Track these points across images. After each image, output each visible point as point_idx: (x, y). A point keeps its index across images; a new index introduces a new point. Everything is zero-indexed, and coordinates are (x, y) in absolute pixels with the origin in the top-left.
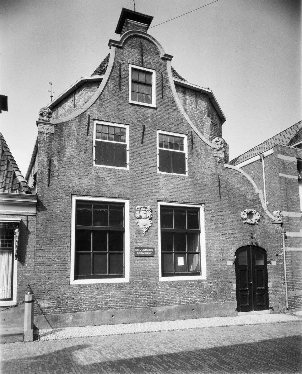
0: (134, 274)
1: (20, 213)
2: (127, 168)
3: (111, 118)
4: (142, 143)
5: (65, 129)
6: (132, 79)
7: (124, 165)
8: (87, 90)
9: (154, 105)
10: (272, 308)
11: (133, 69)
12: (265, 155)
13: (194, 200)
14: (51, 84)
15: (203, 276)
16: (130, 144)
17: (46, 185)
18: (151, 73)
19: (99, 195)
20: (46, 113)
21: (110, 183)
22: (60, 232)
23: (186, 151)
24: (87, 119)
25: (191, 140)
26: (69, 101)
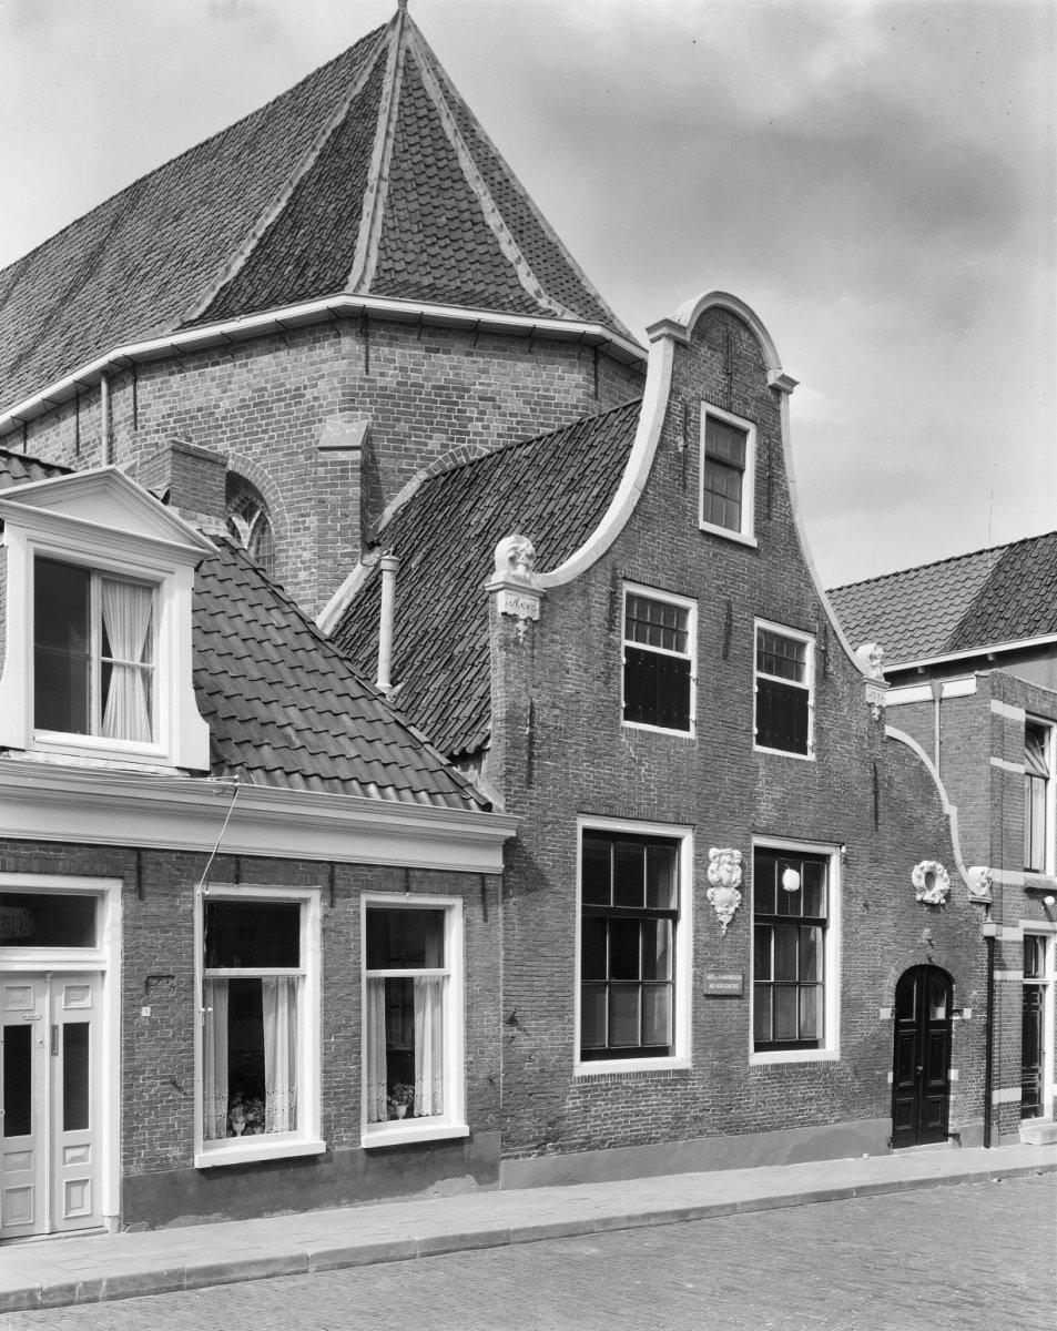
2: (691, 734)
4: (725, 657)
5: (562, 607)
6: (706, 452)
10: (956, 1136)
11: (710, 417)
15: (682, 1055)
16: (700, 660)
19: (635, 814)
20: (523, 554)
22: (552, 923)
23: (808, 681)
25: (822, 655)
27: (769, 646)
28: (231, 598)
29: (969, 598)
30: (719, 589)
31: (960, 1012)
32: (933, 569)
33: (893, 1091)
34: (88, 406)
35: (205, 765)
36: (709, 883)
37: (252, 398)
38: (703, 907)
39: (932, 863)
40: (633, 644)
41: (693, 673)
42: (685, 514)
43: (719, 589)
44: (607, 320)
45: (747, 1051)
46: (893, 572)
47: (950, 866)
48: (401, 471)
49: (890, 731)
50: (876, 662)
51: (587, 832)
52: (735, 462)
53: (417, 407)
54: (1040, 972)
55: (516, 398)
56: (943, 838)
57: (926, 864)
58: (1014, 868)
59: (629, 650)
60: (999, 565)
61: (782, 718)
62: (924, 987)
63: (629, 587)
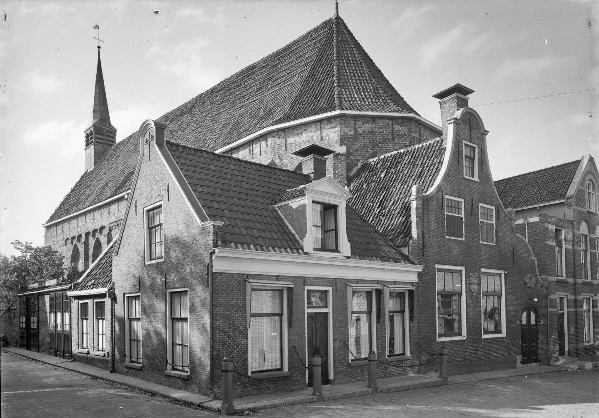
10: (540, 361)
16: (465, 217)
28: (267, 187)
30: (469, 195)
31: (540, 322)
35: (349, 255)
37: (309, 140)
40: (482, 220)
43: (469, 195)
44: (411, 110)
45: (305, 309)
48: (356, 160)
53: (361, 140)
56: (533, 268)
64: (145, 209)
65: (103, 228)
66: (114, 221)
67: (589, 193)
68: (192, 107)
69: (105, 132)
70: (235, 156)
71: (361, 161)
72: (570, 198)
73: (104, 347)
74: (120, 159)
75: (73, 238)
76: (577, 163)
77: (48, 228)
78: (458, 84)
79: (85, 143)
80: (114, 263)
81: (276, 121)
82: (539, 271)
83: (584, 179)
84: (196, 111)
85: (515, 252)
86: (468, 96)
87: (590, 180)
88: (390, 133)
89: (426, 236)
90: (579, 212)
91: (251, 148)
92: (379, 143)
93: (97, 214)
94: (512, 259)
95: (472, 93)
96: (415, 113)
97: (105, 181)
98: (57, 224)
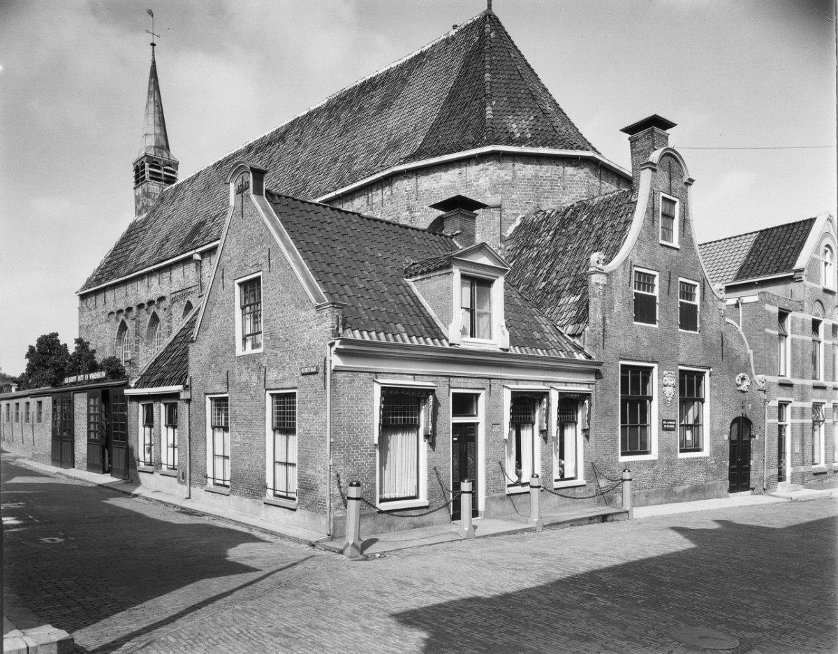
0: (661, 451)
1: (427, 372)
3: (647, 264)
7: (654, 322)
8: (495, 166)
9: (675, 244)
10: (753, 489)
12: (744, 302)
13: (703, 363)
14: (152, 16)
15: (706, 452)
17: (601, 348)
18: (675, 202)
21: (645, 343)
24: (629, 265)
25: (703, 288)
26: (449, 172)
27: (683, 287)
29: (743, 256)
31: (754, 437)
32: (723, 242)
33: (729, 470)
34: (377, 190)
36: (662, 388)
38: (662, 394)
39: (744, 374)
40: (637, 291)
41: (658, 301)
42: (654, 237)
46: (704, 243)
47: (751, 376)
48: (514, 214)
49: (728, 320)
50: (722, 292)
51: (622, 366)
52: (671, 214)
54: (784, 419)
55: (575, 187)
56: (747, 365)
57: (741, 375)
58: (774, 375)
59: (681, 303)
60: (756, 241)
61: (688, 318)
62: (743, 425)
63: (636, 269)
64: (453, 391)
65: (162, 299)
66: (178, 289)
67: (826, 264)
68: (286, 132)
69: (162, 163)
70: (346, 207)
71: (521, 216)
72: (801, 270)
73: (176, 464)
74: (185, 203)
75: (120, 311)
76: (811, 221)
77: (83, 297)
78: (655, 115)
79: (134, 180)
80: (191, 354)
81: (406, 158)
82: (756, 368)
83: (820, 242)
84: (290, 138)
85: (725, 342)
86: (668, 131)
87: (828, 246)
88: (560, 178)
89: (608, 321)
90: (812, 289)
91: (370, 195)
92: (544, 192)
93: (154, 281)
94: (720, 352)
95: (673, 127)
96: (594, 149)
97: (161, 236)
98: (96, 293)
